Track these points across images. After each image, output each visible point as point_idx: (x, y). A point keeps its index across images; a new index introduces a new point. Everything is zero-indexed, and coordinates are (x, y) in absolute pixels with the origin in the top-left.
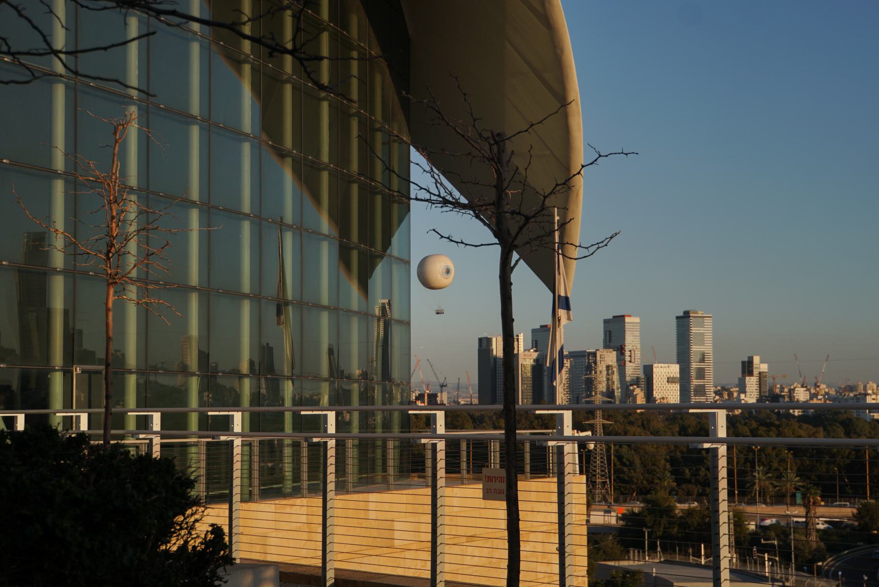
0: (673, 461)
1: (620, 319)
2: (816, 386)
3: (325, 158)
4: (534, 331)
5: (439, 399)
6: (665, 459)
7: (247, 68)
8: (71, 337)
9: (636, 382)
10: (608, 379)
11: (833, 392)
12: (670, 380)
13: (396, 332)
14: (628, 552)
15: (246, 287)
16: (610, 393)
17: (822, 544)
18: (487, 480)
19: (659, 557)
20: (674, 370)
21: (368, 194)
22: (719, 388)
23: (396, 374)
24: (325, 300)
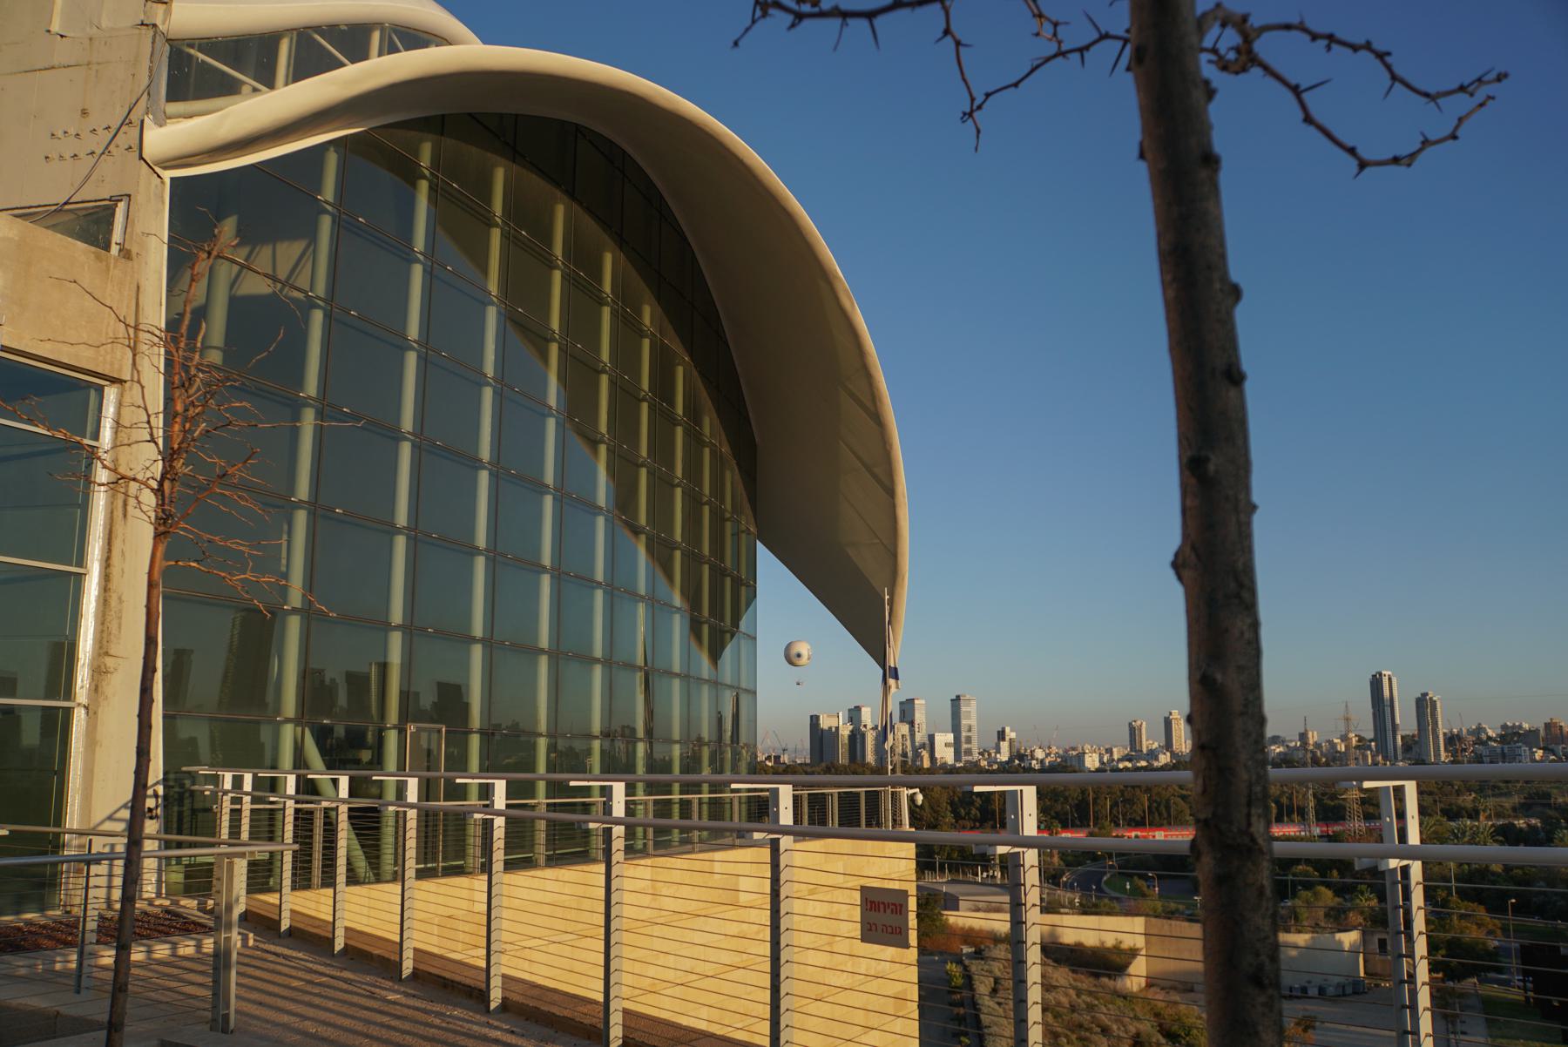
0: (952, 803)
1: (911, 701)
2: (1049, 748)
3: (678, 537)
4: (849, 710)
5: (782, 760)
6: (947, 803)
7: (603, 449)
8: (405, 696)
9: (923, 746)
10: (903, 745)
11: (1061, 752)
12: (947, 745)
13: (745, 700)
14: (924, 873)
15: (598, 652)
16: (904, 754)
17: (1062, 863)
18: (869, 907)
19: (947, 877)
20: (950, 737)
21: (718, 573)
22: (981, 750)
23: (743, 739)
24: (677, 668)
